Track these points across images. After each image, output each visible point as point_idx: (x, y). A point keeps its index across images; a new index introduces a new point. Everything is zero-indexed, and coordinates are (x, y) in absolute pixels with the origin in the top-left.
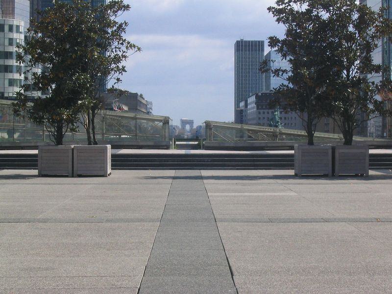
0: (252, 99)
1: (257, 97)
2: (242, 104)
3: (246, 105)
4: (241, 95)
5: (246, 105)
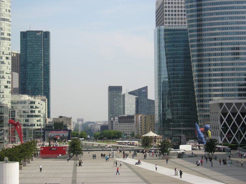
0: (116, 118)
1: (119, 118)
2: (112, 119)
3: (114, 120)
5: (114, 120)
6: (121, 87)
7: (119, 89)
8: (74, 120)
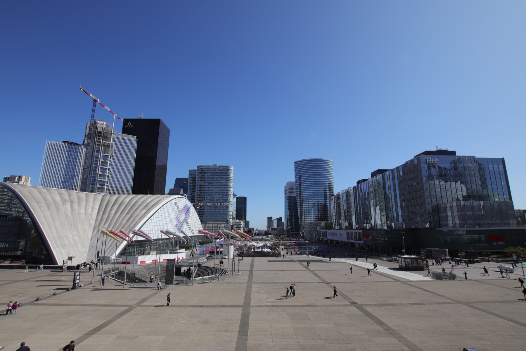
4: (269, 227)
6: (245, 198)
7: (271, 218)
8: (255, 229)
